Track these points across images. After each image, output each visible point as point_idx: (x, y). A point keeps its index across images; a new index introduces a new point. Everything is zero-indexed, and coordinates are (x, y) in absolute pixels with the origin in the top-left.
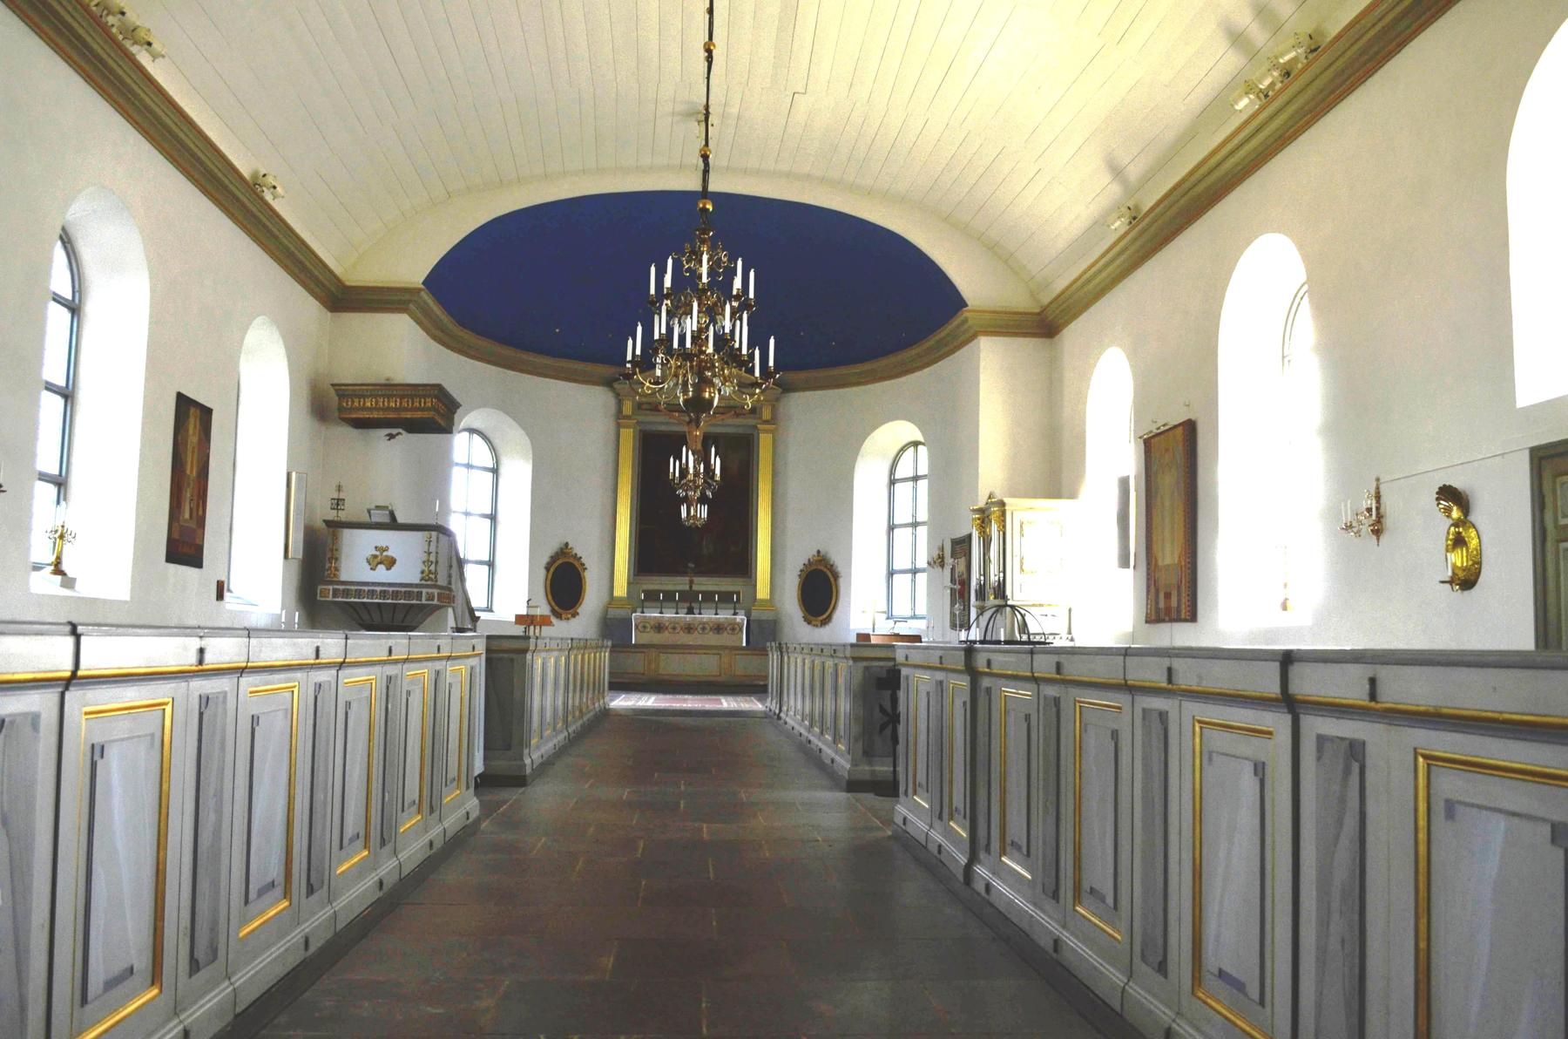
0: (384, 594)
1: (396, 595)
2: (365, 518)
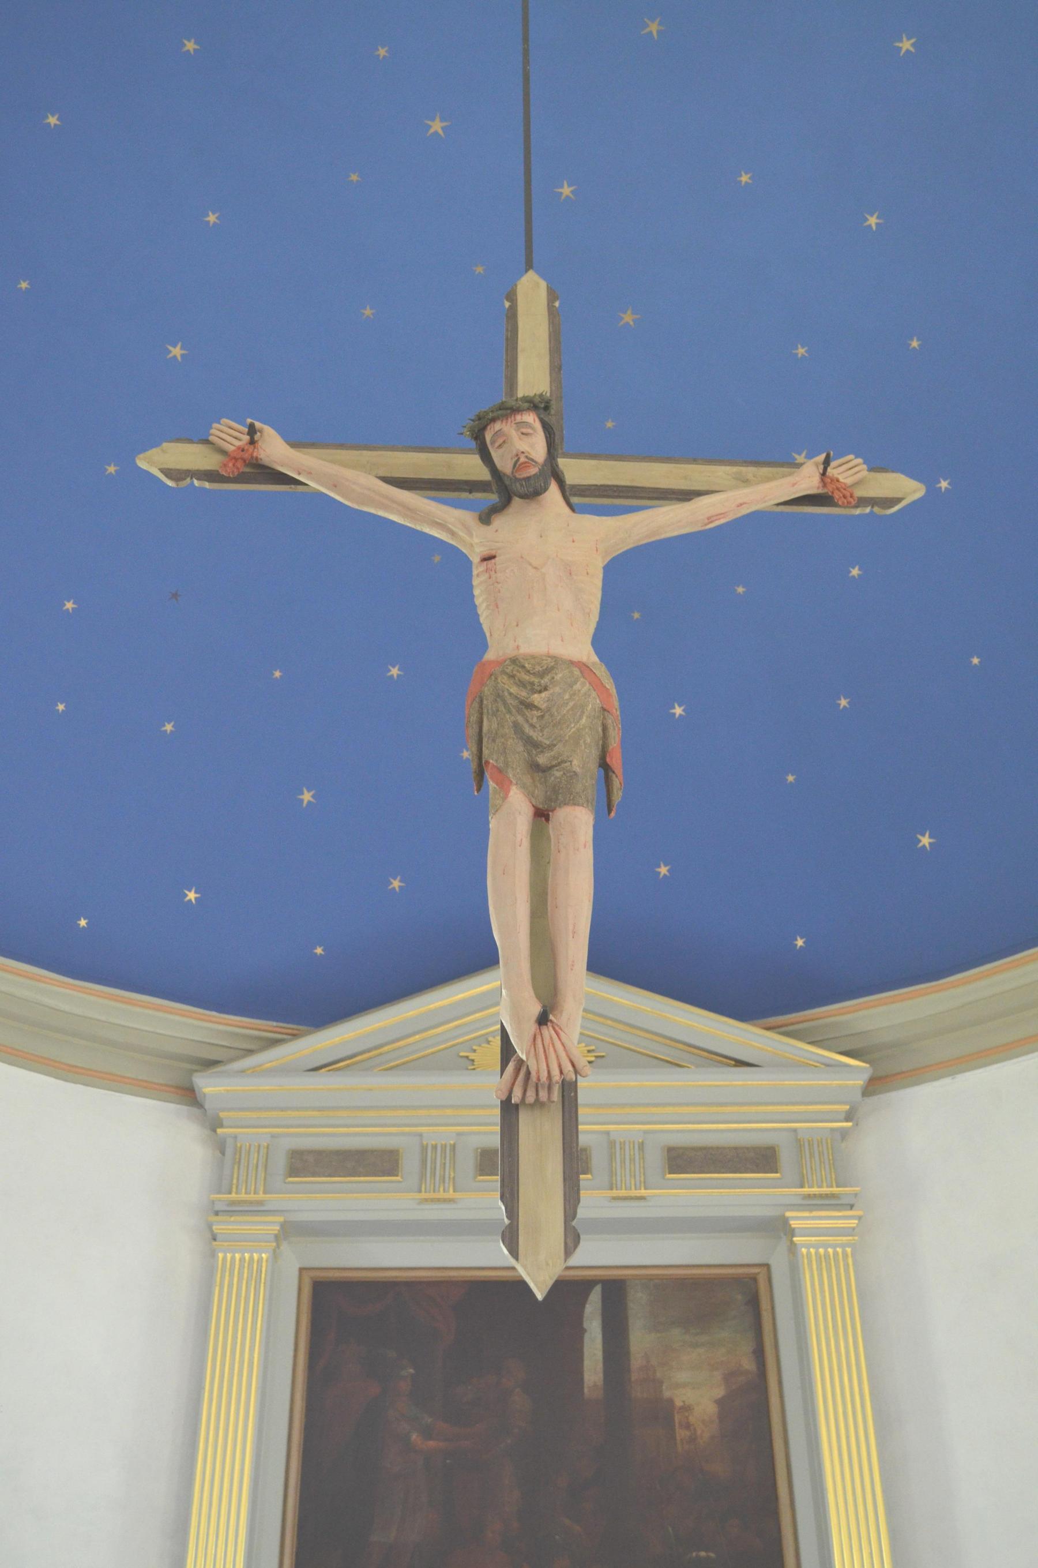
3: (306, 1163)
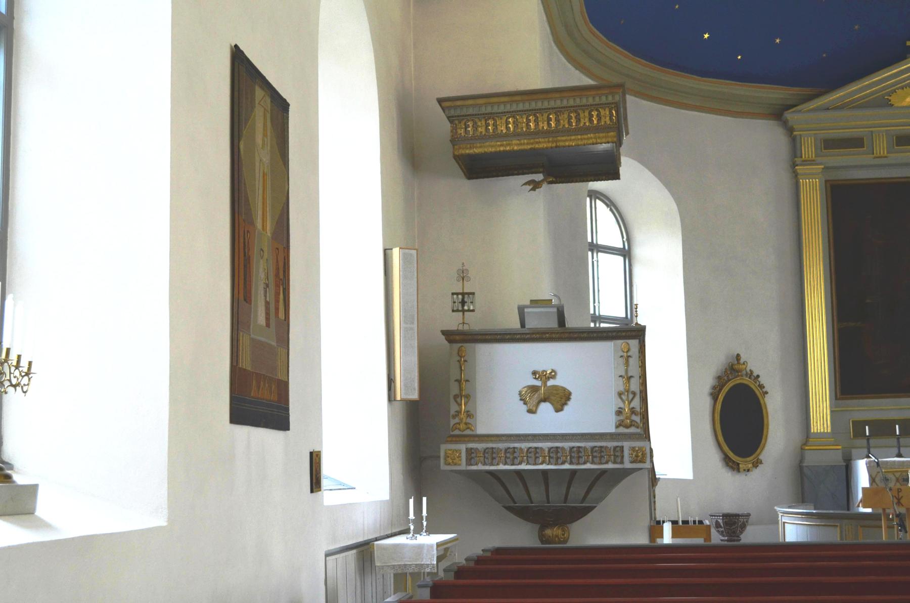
0: (555, 455)
1: (576, 455)
2: (513, 323)
3: (830, 144)
